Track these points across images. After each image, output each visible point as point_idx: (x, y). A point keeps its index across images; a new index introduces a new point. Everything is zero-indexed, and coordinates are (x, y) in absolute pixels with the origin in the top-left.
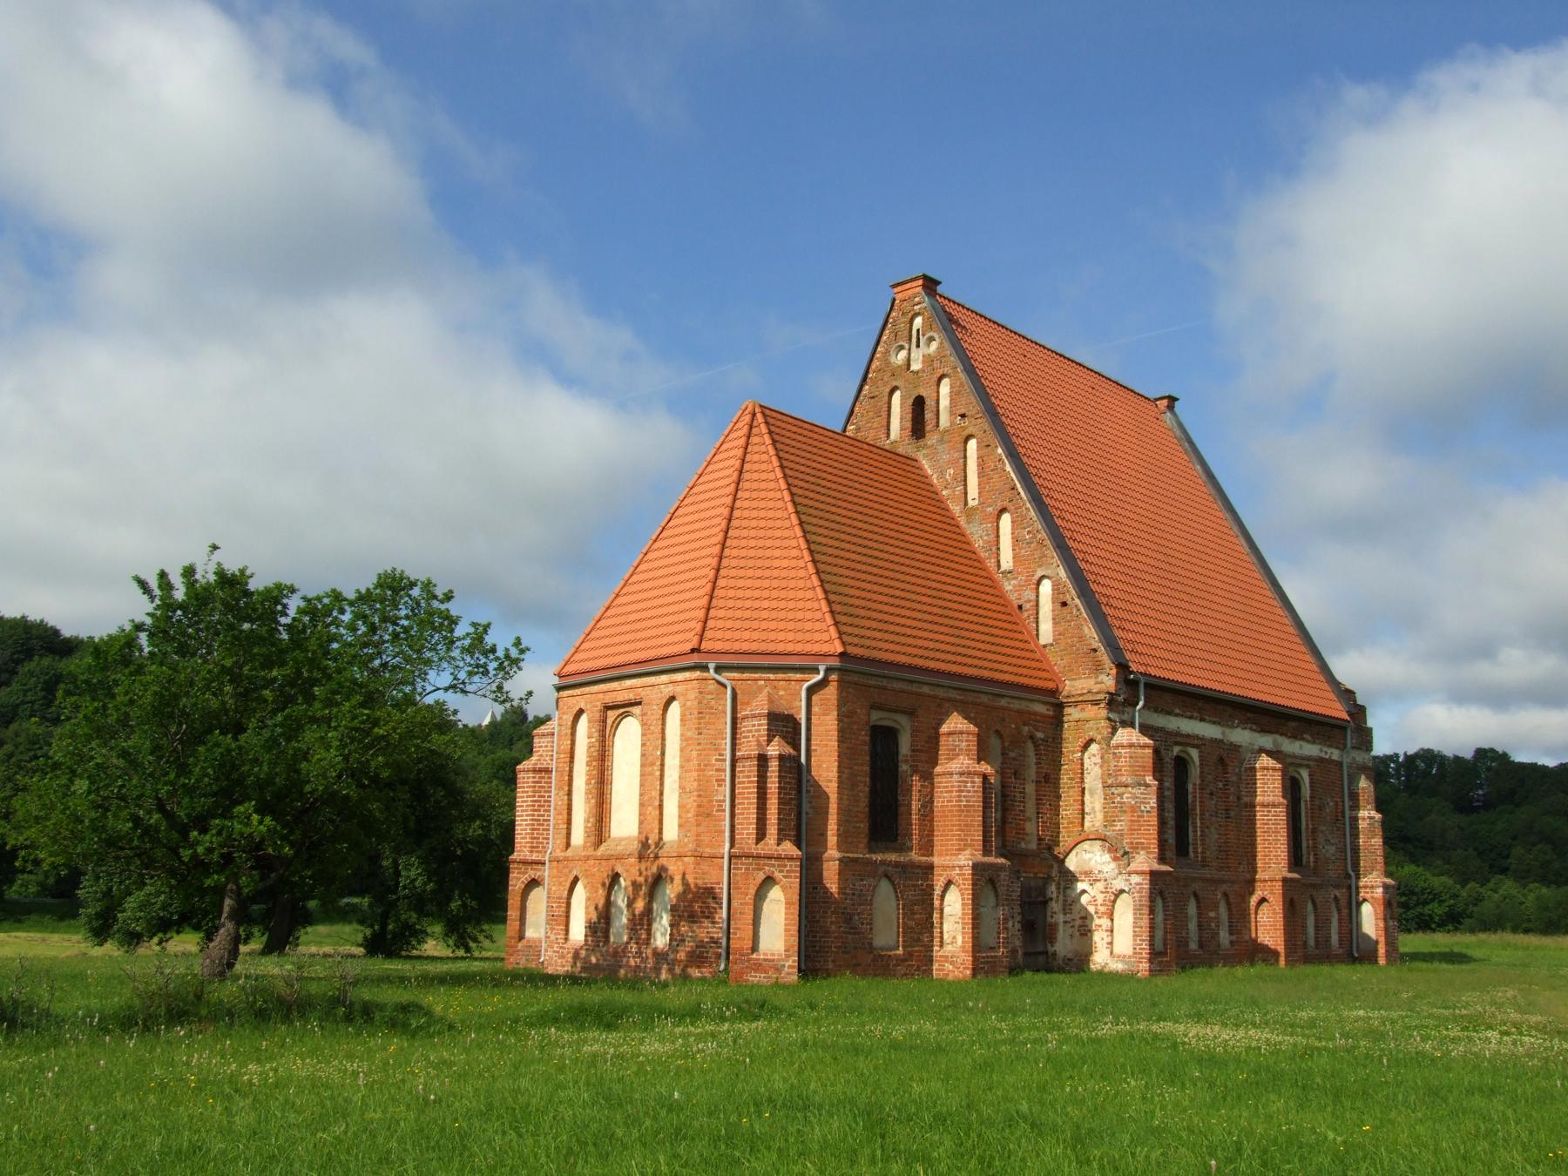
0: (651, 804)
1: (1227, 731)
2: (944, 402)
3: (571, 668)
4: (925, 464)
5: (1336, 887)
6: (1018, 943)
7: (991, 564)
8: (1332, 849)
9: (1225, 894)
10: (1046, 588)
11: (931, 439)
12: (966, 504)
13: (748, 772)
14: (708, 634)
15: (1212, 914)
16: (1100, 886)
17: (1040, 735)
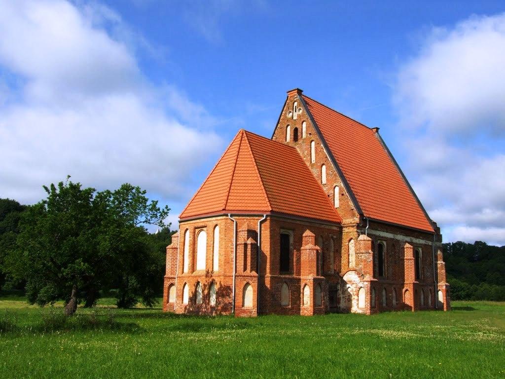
0: (210, 260)
1: (395, 235)
2: (304, 130)
3: (184, 215)
4: (298, 150)
5: (431, 286)
6: (328, 304)
7: (319, 182)
8: (429, 274)
9: (395, 288)
10: (337, 189)
11: (300, 141)
12: (311, 162)
13: (241, 249)
14: (228, 204)
15: (390, 295)
16: (354, 285)
17: (335, 237)
